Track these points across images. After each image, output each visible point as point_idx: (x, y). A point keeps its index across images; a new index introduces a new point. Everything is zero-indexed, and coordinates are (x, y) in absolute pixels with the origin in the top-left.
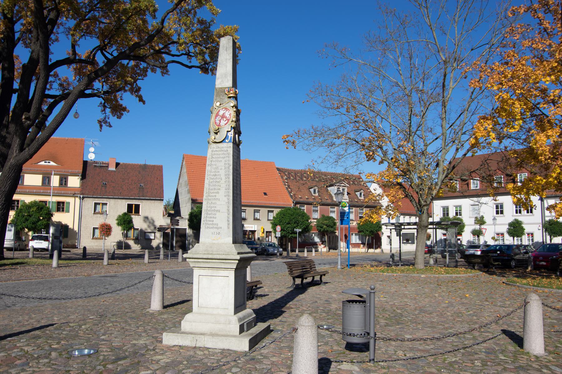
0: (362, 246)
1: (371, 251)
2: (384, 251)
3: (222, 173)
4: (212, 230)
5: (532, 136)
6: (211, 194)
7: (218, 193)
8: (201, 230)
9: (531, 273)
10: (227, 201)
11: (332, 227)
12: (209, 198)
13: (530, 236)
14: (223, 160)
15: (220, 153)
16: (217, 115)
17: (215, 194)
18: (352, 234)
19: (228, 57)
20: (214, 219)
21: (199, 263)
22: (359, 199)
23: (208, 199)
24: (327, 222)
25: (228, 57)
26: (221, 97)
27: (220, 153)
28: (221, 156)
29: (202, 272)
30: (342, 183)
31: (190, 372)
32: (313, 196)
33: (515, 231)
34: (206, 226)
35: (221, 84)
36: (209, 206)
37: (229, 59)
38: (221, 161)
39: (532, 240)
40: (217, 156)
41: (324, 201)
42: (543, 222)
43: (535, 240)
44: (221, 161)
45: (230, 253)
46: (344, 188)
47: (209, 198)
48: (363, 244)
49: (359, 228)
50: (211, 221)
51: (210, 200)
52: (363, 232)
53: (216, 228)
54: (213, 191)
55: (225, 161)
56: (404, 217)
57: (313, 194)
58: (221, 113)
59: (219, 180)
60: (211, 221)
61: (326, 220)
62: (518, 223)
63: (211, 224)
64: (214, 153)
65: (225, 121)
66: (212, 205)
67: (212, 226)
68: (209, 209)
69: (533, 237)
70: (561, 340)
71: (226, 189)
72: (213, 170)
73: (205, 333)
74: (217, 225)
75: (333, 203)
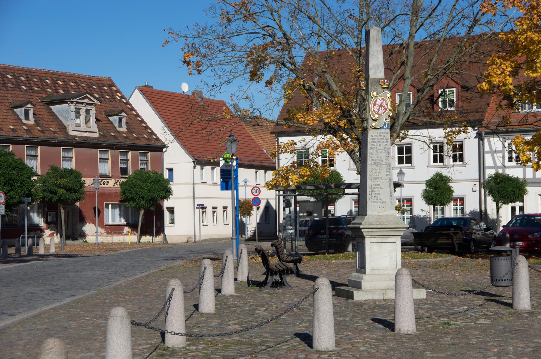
0: (127, 229)
1: (146, 239)
2: (169, 241)
4: (377, 204)
5: (491, 56)
6: (374, 174)
7: (380, 172)
8: (368, 204)
9: (40, 350)
11: (76, 192)
12: (373, 177)
13: (458, 203)
14: (383, 145)
15: (379, 138)
16: (375, 104)
17: (377, 174)
18: (107, 206)
19: (378, 49)
20: (378, 195)
21: (372, 233)
22: (119, 132)
23: (372, 178)
24: (67, 180)
25: (378, 49)
26: (376, 87)
27: (379, 138)
28: (381, 141)
29: (373, 240)
30: (87, 97)
32: (25, 125)
33: (437, 195)
34: (372, 201)
35: (374, 74)
37: (380, 51)
38: (381, 145)
39: (462, 210)
40: (377, 141)
41: (48, 136)
42: (482, 181)
43: (467, 210)
44: (381, 145)
45: (398, 223)
46: (89, 107)
47: (373, 177)
48: (133, 226)
49: (124, 193)
50: (376, 197)
51: (374, 178)
52: (133, 199)
53: (381, 202)
54: (375, 171)
55: (385, 145)
56: (202, 169)
57: (24, 121)
58: (379, 102)
59: (380, 162)
60: (376, 197)
61: (64, 177)
62: (442, 180)
64: (373, 138)
65: (383, 110)
66: (376, 183)
67: (377, 201)
69: (463, 204)
71: (387, 170)
72: (374, 153)
73: (166, 342)
74: (382, 200)
75: (70, 140)
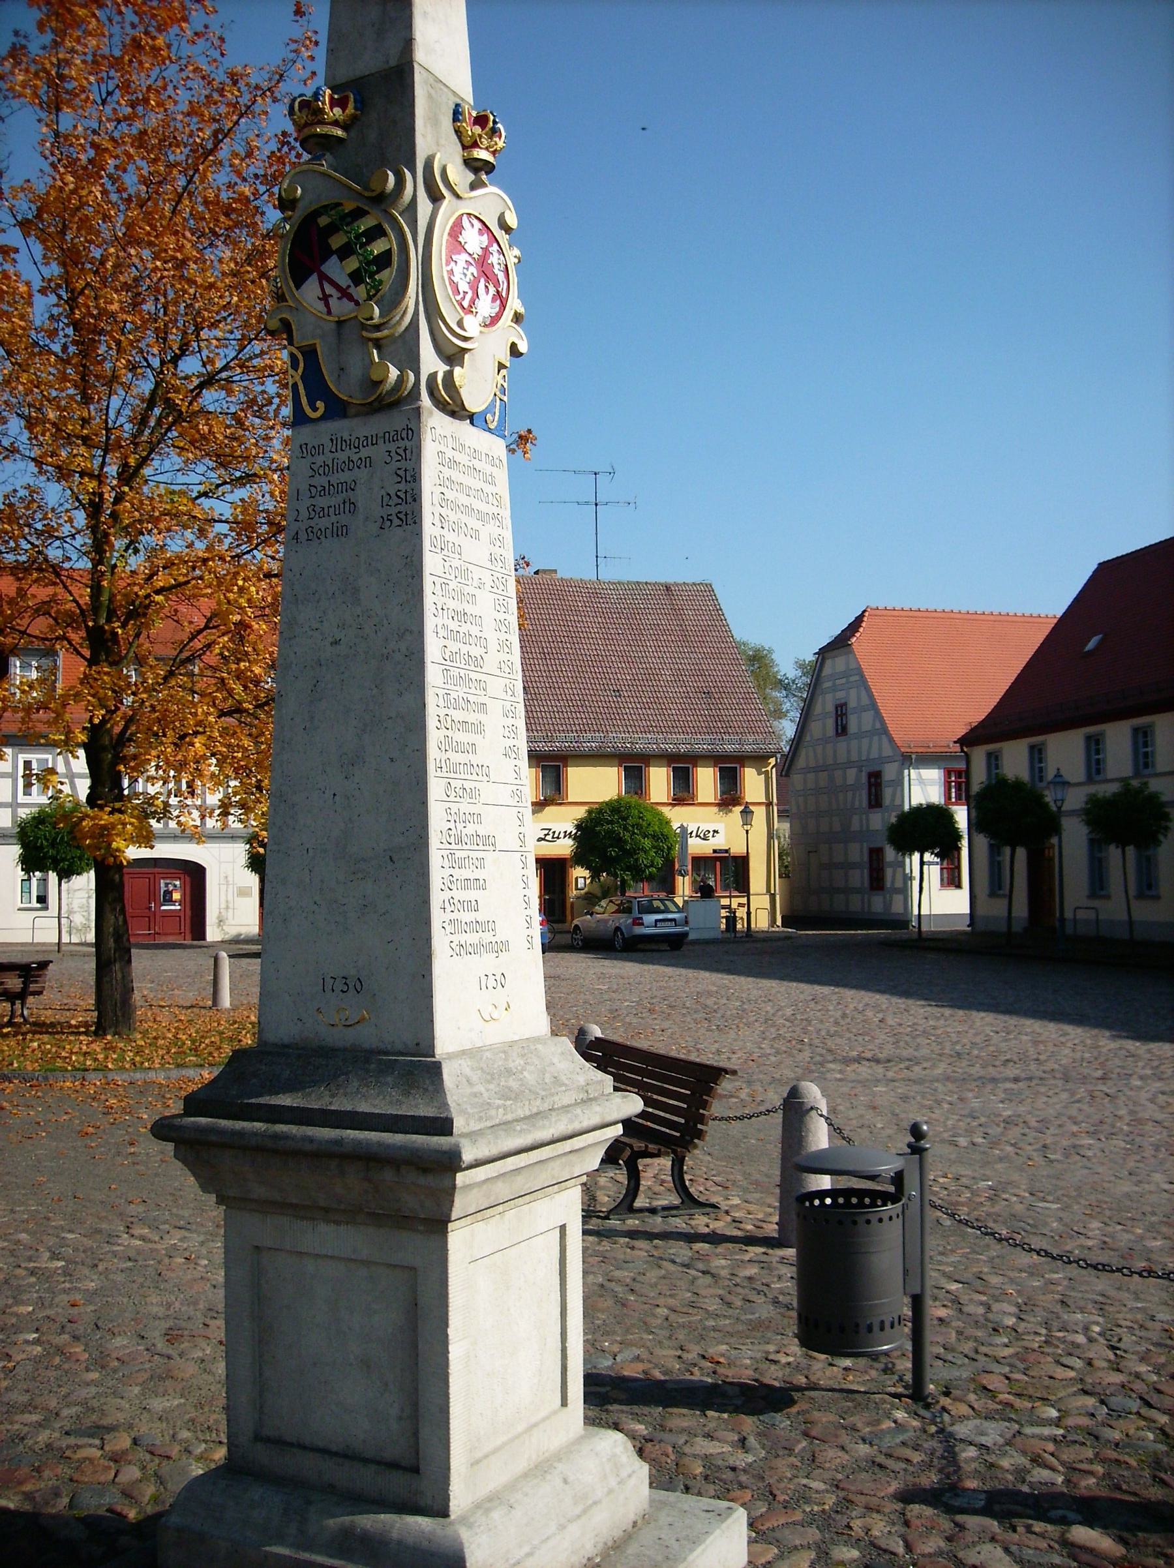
7: (479, 728)
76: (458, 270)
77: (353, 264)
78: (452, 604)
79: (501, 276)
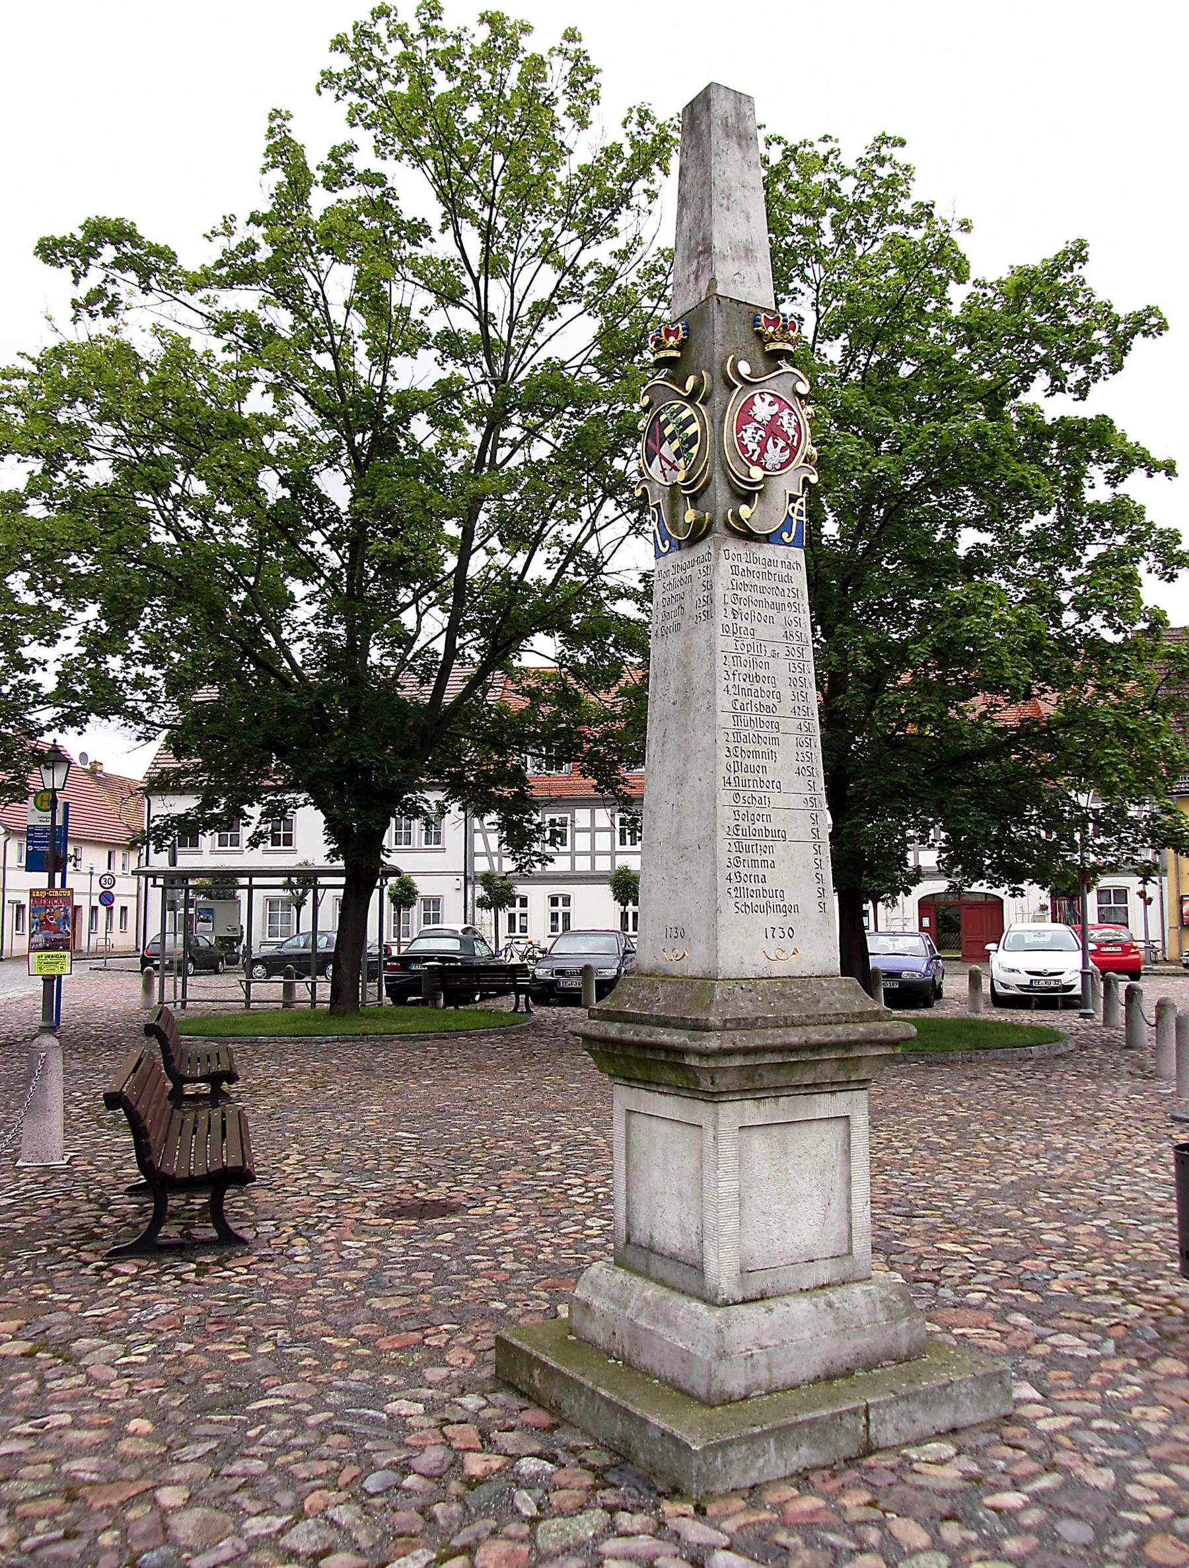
3: (781, 668)
7: (771, 755)
10: (805, 789)
31: (630, 1557)
34: (741, 901)
36: (743, 811)
53: (778, 909)
63: (757, 893)
67: (761, 901)
68: (744, 825)
70: (2, 1537)
76: (747, 436)
77: (676, 444)
78: (743, 670)
79: (791, 432)
